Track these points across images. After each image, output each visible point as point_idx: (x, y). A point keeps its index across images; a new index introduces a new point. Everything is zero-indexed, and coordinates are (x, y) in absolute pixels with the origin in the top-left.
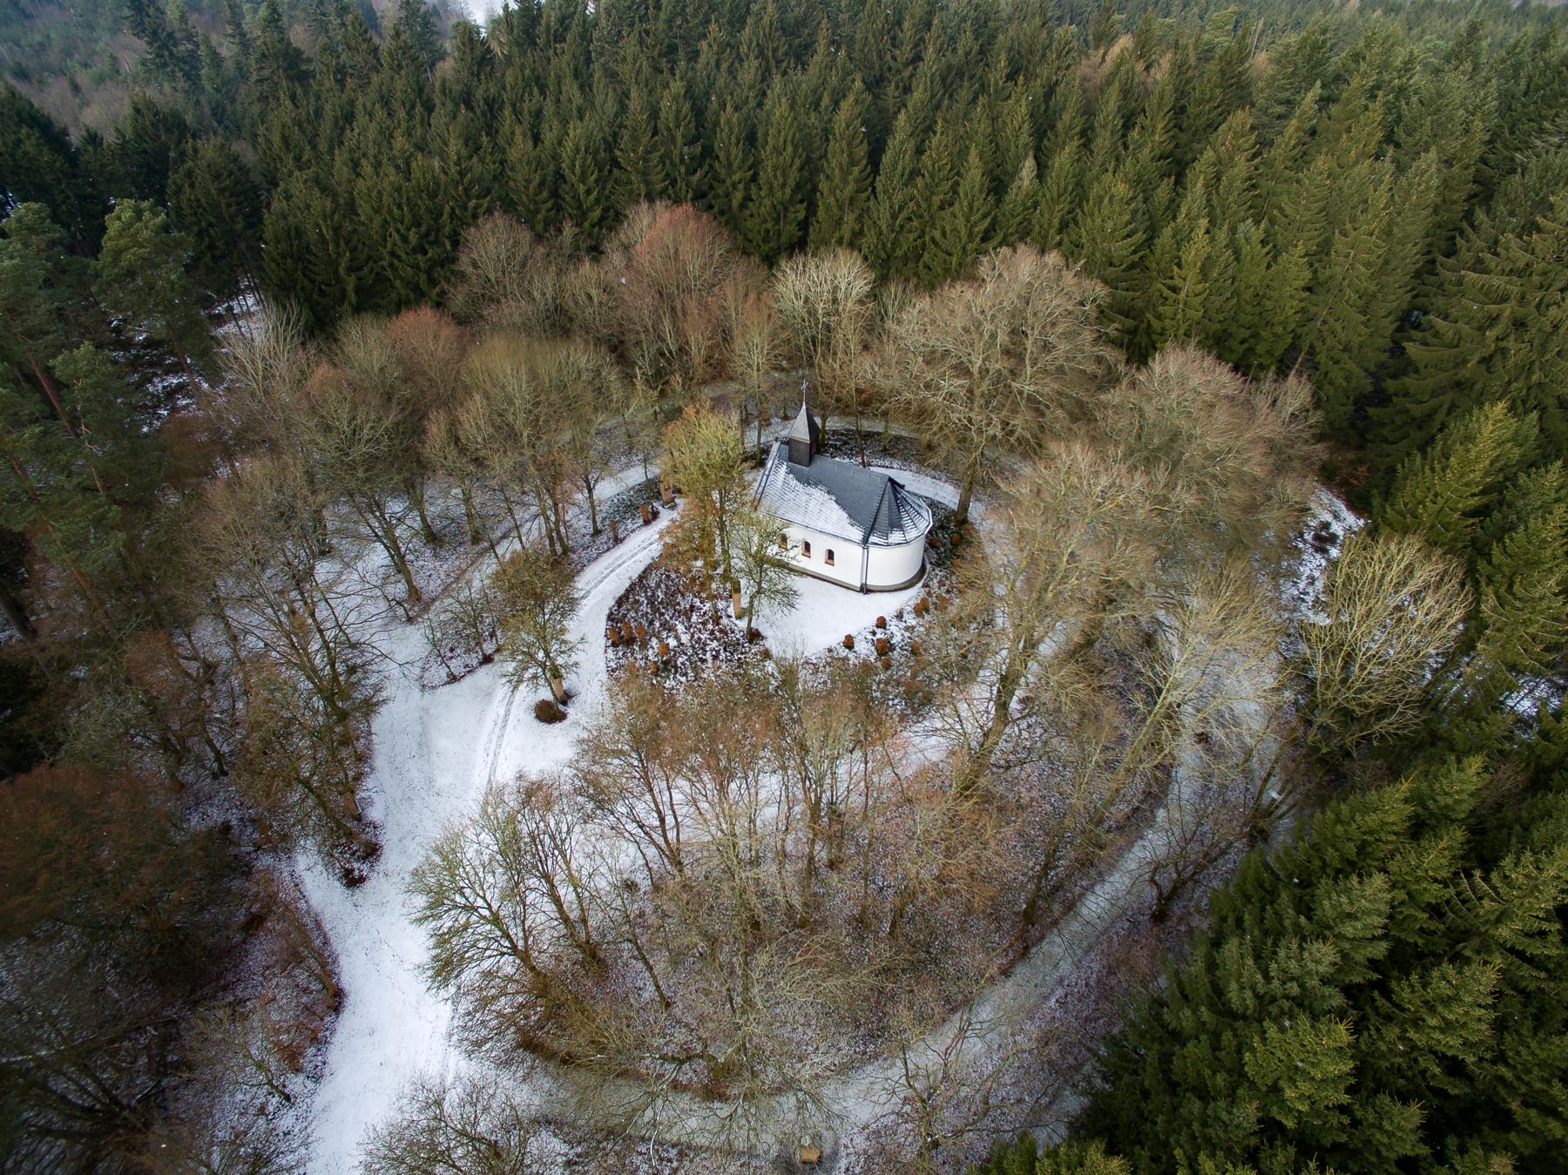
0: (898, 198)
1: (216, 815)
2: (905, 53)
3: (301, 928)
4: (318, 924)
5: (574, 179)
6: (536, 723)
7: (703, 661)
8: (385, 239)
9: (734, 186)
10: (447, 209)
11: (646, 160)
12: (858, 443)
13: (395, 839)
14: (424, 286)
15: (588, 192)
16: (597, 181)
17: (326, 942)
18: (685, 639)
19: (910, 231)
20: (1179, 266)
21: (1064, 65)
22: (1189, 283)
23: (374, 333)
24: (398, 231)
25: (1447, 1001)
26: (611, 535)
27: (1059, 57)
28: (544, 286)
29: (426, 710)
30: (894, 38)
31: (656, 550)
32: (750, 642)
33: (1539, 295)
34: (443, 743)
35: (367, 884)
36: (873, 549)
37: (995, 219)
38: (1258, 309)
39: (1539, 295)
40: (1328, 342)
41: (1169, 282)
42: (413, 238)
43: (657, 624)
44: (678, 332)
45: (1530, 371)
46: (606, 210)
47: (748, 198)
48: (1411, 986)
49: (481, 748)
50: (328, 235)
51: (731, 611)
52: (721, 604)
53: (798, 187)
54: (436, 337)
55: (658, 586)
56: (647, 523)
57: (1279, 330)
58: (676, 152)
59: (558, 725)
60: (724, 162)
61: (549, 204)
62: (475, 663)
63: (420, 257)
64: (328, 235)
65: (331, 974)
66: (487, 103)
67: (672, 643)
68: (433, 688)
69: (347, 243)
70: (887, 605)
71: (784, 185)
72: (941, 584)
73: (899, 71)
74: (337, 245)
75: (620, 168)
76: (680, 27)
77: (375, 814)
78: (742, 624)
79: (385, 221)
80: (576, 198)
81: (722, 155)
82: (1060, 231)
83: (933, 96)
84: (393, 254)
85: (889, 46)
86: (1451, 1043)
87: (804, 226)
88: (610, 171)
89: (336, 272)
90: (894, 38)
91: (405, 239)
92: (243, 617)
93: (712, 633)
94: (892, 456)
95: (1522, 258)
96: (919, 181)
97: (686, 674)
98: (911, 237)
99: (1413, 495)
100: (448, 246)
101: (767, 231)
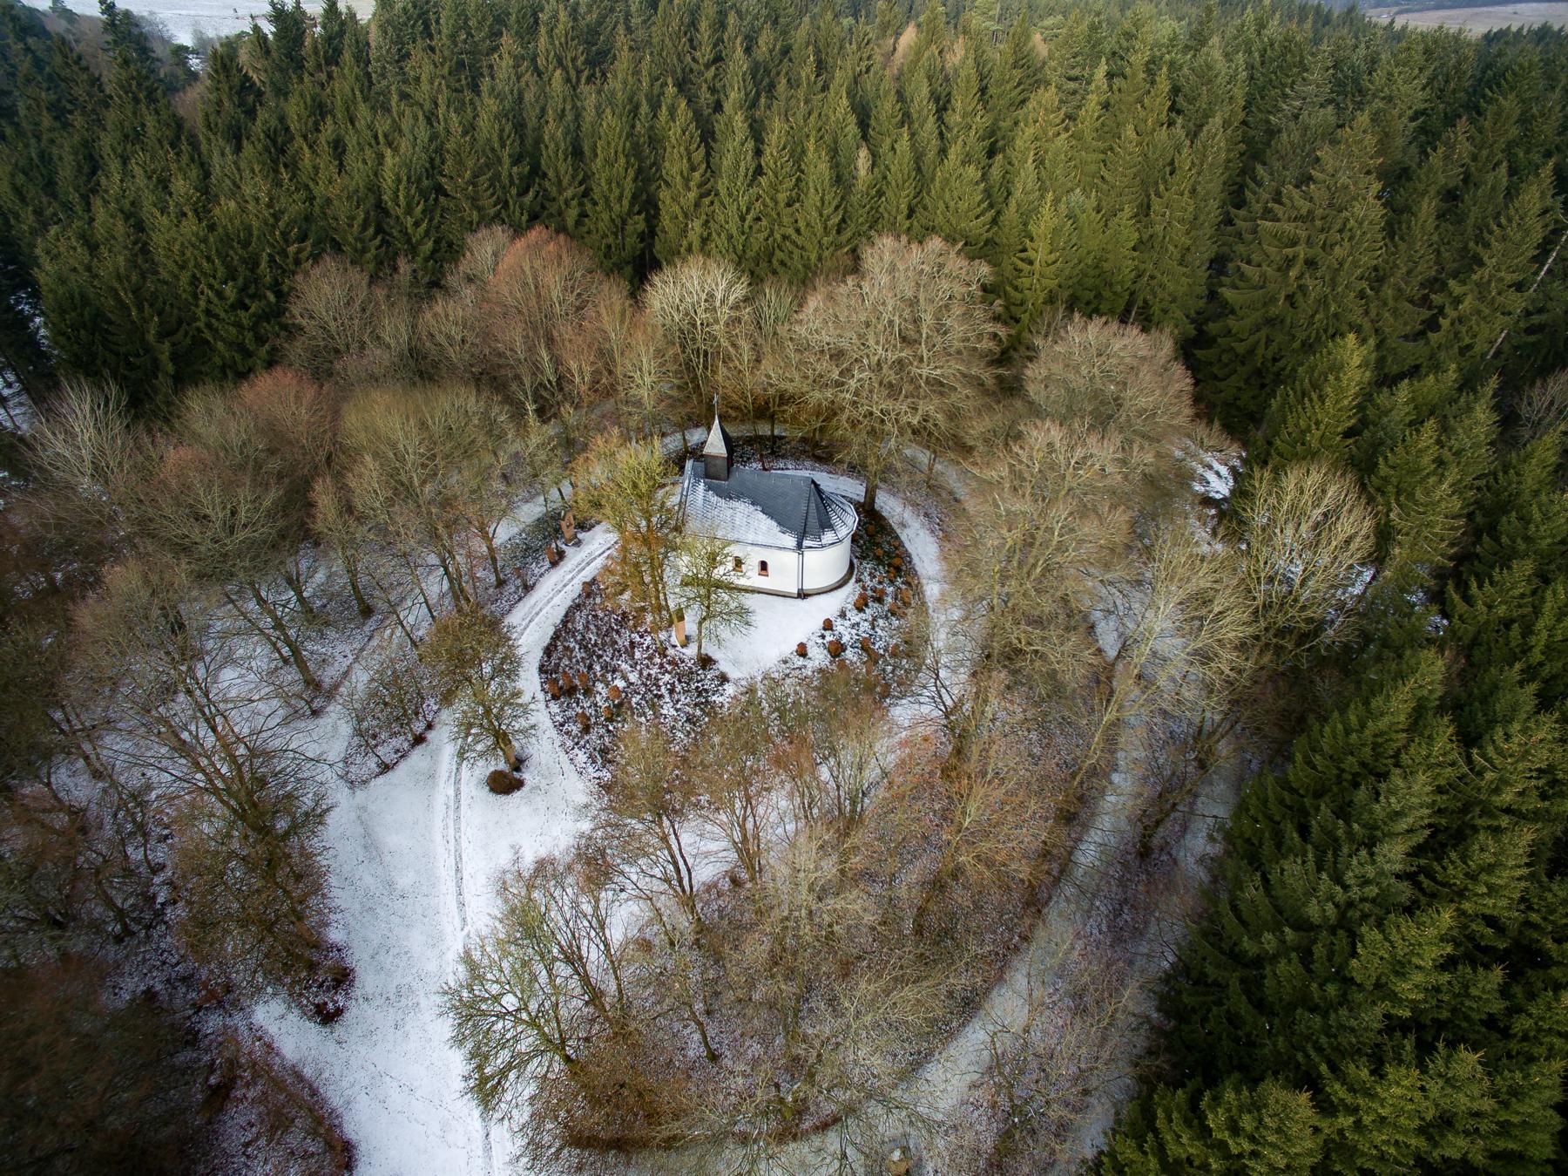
0: (743, 202)
1: (131, 986)
2: (705, 53)
3: (278, 1084)
4: (299, 1077)
5: (400, 212)
6: (492, 797)
7: (660, 697)
8: (195, 297)
9: (567, 203)
10: (265, 258)
11: (475, 185)
12: (772, 449)
13: (366, 957)
14: (251, 346)
15: (417, 224)
16: (424, 212)
17: (314, 1092)
18: (633, 677)
19: (759, 231)
20: (1032, 240)
21: (865, 55)
22: (1040, 253)
23: (218, 404)
24: (211, 287)
25: (1490, 869)
26: (518, 582)
27: (859, 49)
28: (394, 329)
29: (364, 809)
30: (691, 40)
31: (575, 589)
32: (704, 668)
33: (1323, 237)
34: (393, 839)
35: (346, 1015)
36: (807, 553)
37: (846, 211)
38: (1097, 272)
39: (1323, 237)
40: (1160, 296)
41: (1023, 255)
42: (229, 290)
43: (598, 668)
44: (557, 361)
45: (1326, 305)
46: (437, 242)
47: (583, 215)
48: (1452, 862)
49: (438, 837)
50: (128, 298)
51: (674, 640)
52: (663, 636)
53: (635, 197)
54: (297, 397)
55: (587, 627)
56: (554, 564)
57: (1118, 288)
58: (505, 174)
59: (517, 794)
60: (554, 180)
61: (377, 242)
62: (406, 745)
63: (241, 313)
64: (128, 298)
65: (332, 1128)
66: (268, 136)
67: (620, 684)
68: (364, 782)
69: (151, 305)
70: (829, 605)
71: (620, 199)
72: (872, 576)
73: (701, 73)
74: (141, 309)
75: (446, 195)
76: (465, 42)
77: (335, 935)
78: (691, 651)
79: (194, 276)
80: (404, 232)
81: (551, 174)
82: (909, 217)
83: (747, 95)
84: (208, 312)
85: (687, 47)
86: (1490, 905)
87: (649, 235)
88: (436, 200)
89: (143, 340)
90: (691, 40)
91: (220, 295)
92: (115, 747)
93: (661, 666)
94: (783, 457)
95: (1305, 206)
96: (763, 180)
97: (644, 714)
98: (761, 237)
99: (1297, 425)
100: (272, 298)
101: (609, 247)
